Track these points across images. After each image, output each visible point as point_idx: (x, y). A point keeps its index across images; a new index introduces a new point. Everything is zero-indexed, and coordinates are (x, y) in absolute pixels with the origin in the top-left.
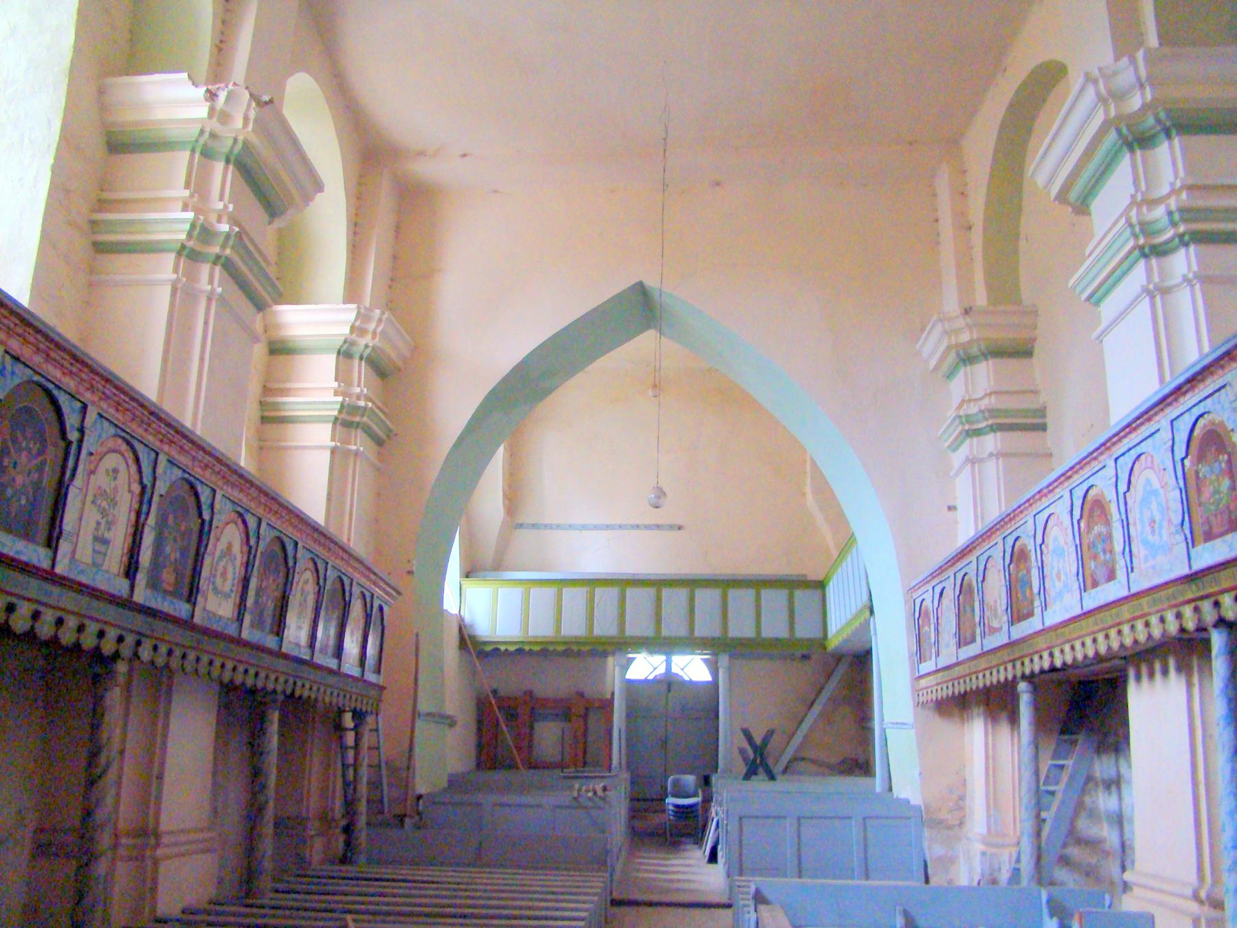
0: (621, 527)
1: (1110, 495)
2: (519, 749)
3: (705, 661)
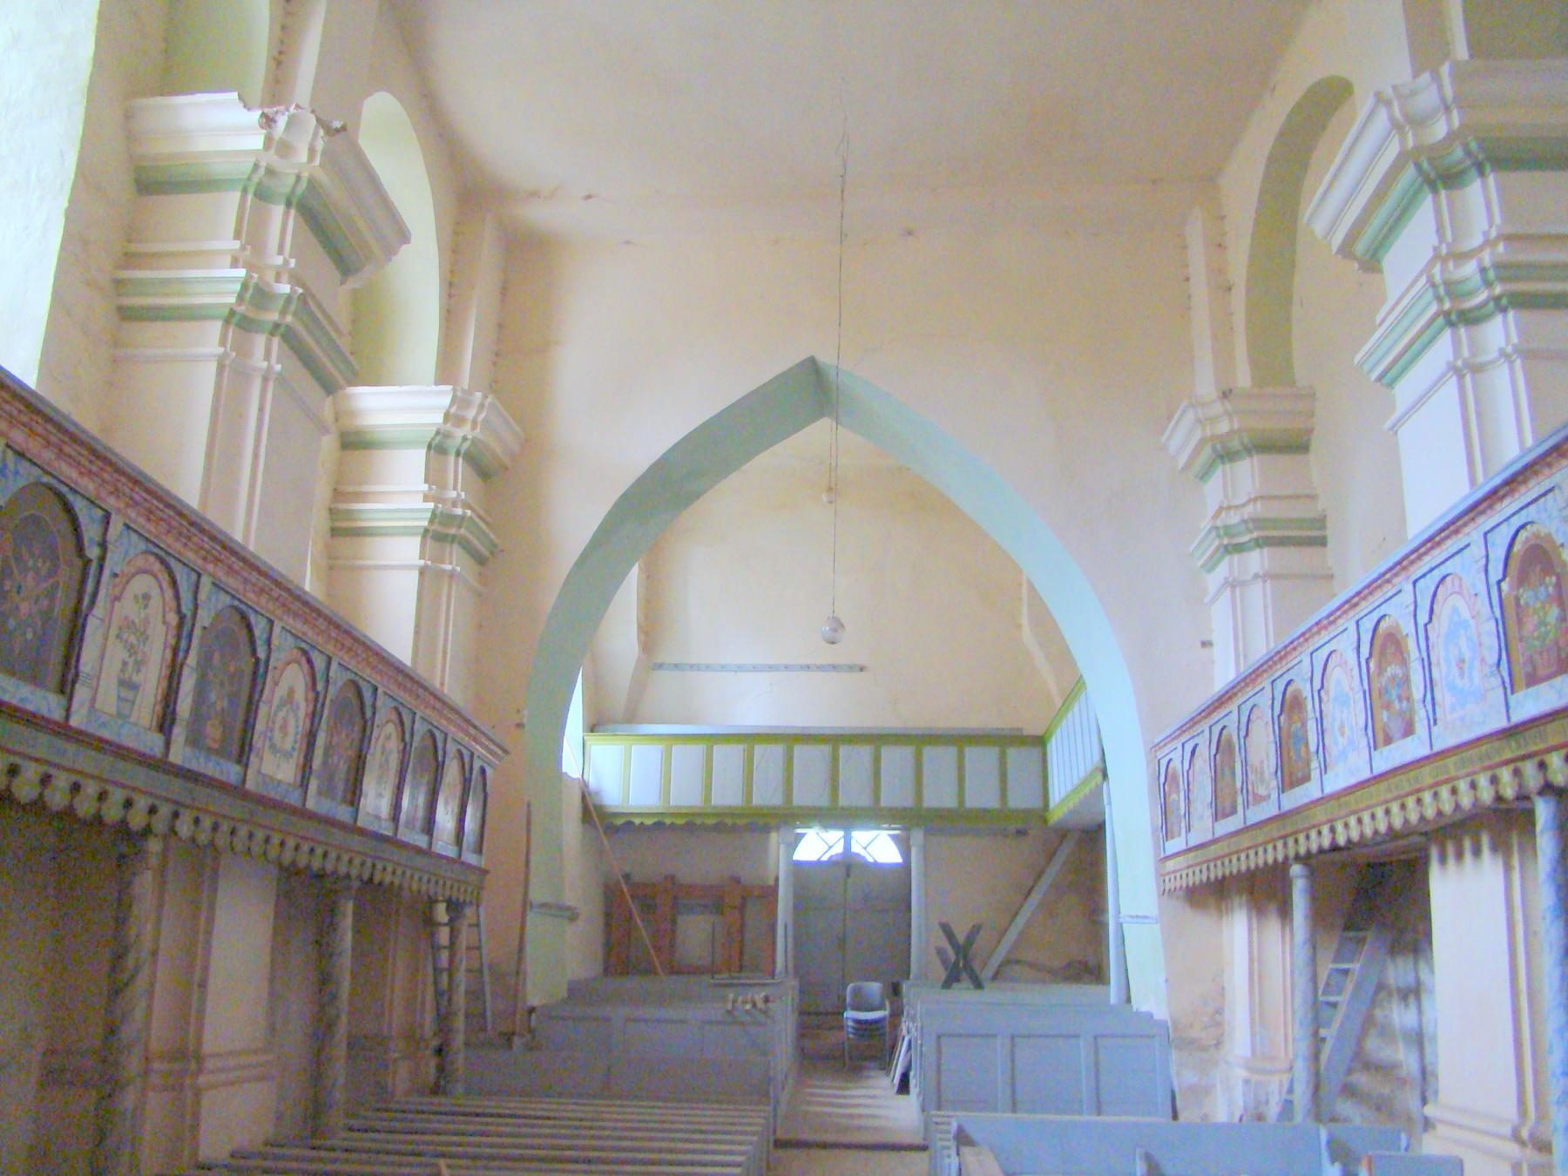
0: (787, 668)
1: (1407, 627)
2: (658, 949)
3: (893, 837)
